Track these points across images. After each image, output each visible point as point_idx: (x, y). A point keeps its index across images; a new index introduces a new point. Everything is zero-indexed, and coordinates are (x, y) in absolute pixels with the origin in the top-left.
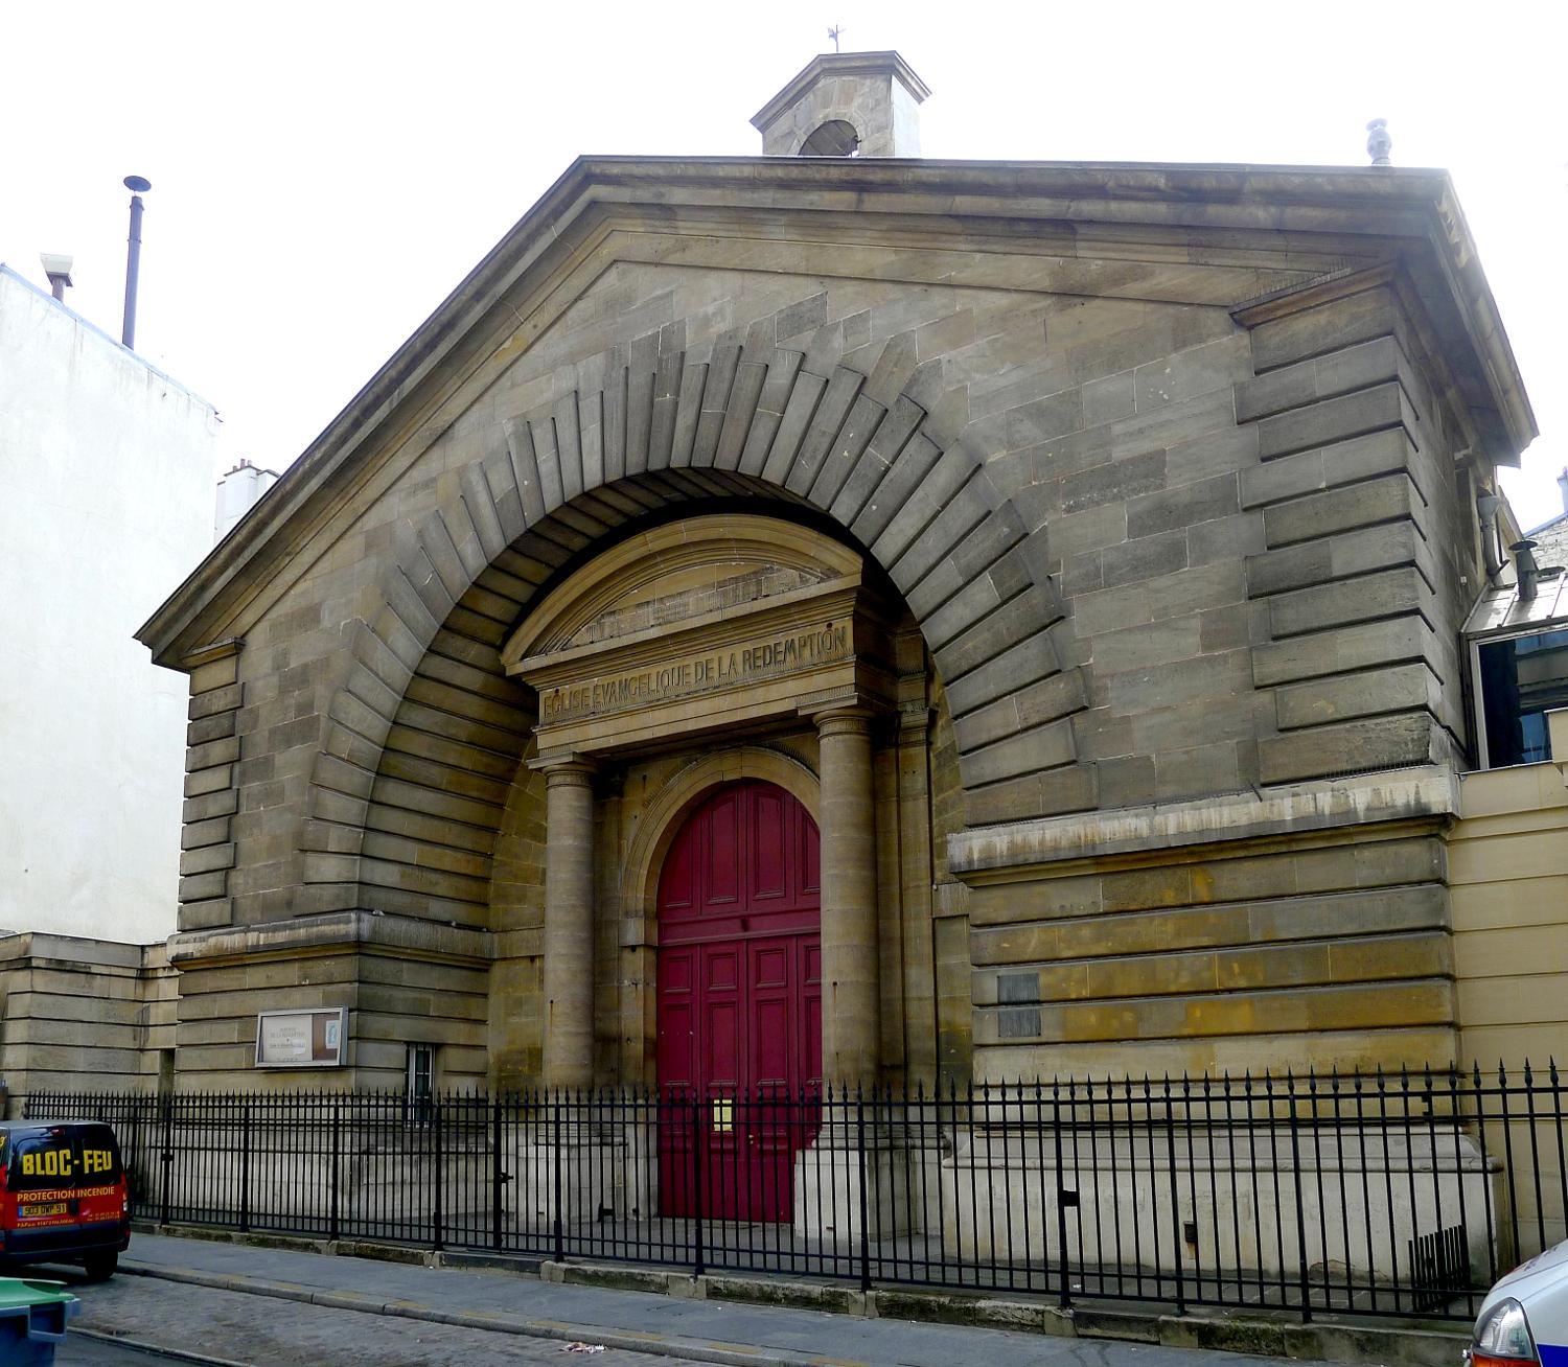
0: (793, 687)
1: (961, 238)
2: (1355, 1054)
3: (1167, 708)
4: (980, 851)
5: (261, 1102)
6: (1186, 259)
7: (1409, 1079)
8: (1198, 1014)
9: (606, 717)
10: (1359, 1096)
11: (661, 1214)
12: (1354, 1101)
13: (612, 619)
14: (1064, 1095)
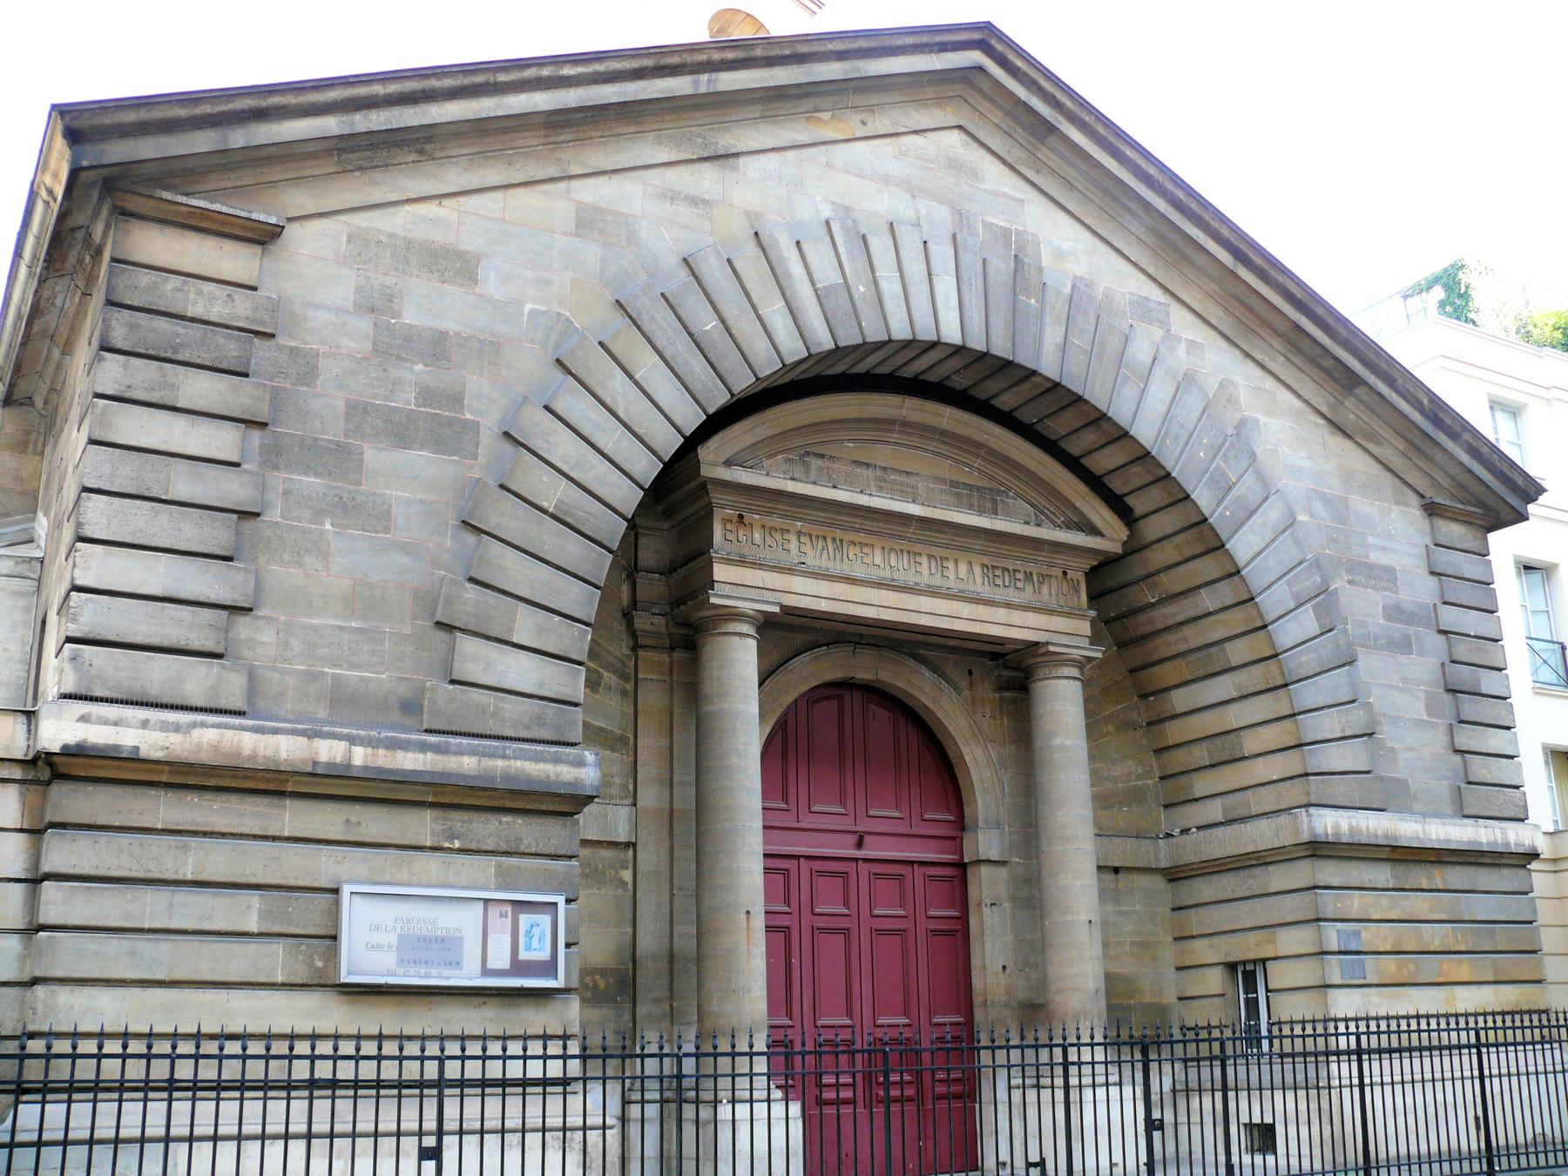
0: (1033, 619)
1: (1279, 339)
2: (1513, 998)
3: (1413, 749)
4: (1332, 828)
5: (1304, 1030)
6: (1402, 448)
7: (446, 1043)
8: (1445, 967)
10: (525, 1058)
12: (560, 1062)
13: (820, 462)
14: (1298, 1030)
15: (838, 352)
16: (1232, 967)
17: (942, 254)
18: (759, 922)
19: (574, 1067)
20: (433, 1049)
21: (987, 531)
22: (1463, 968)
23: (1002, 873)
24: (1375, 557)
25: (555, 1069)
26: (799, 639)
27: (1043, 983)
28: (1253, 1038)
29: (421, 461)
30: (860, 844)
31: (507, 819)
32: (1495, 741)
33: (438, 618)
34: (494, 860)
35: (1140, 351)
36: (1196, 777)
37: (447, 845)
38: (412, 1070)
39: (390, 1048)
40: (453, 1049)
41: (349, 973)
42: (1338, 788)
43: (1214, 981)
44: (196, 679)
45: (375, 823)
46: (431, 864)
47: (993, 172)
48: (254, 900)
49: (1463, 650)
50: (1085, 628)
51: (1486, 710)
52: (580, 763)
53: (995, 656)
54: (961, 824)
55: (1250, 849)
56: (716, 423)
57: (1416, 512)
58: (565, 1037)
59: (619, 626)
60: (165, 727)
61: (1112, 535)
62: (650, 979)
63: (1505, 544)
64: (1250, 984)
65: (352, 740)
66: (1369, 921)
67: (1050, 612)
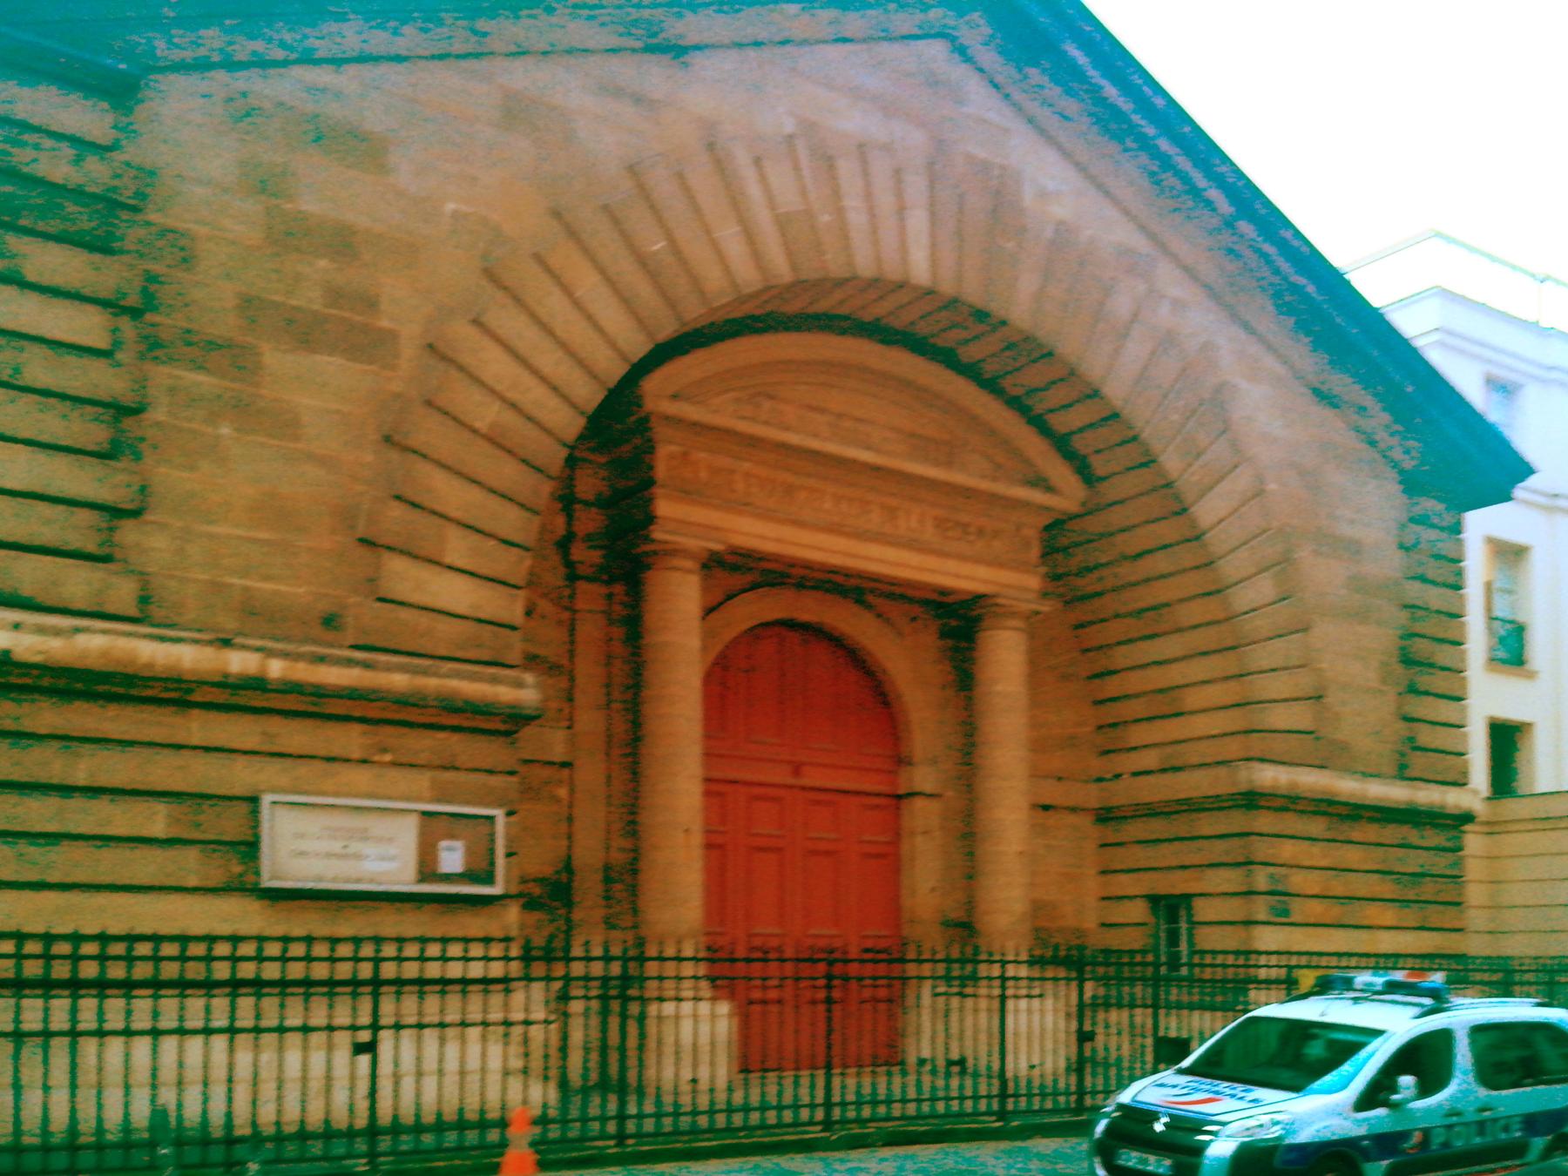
0: (982, 572)
9: (767, 515)
11: (745, 1070)
15: (799, 286)
16: (1154, 900)
17: (916, 187)
18: (697, 839)
19: (515, 968)
20: (367, 950)
21: (947, 484)
22: (1389, 915)
23: (934, 806)
24: (1346, 530)
25: (496, 970)
26: (738, 580)
27: (970, 905)
28: (1174, 963)
29: (329, 365)
30: (797, 770)
31: (442, 735)
32: (1445, 711)
33: (361, 531)
34: (428, 774)
35: (1121, 305)
36: (1134, 728)
37: (376, 758)
38: (344, 971)
39: (321, 950)
40: (389, 950)
41: (272, 878)
42: (1278, 745)
43: (1137, 911)
44: (78, 582)
45: (296, 735)
46: (360, 777)
47: (979, 100)
48: (161, 809)
49: (1427, 626)
50: (1033, 582)
51: (1439, 682)
52: (520, 685)
53: (940, 605)
54: (901, 761)
55: (1182, 796)
56: (663, 353)
57: (1394, 488)
58: (507, 940)
59: (555, 559)
60: (41, 630)
61: (1069, 494)
62: (588, 887)
63: (1481, 524)
64: (1173, 918)
65: (270, 653)
66: (1299, 867)
67: (1001, 565)
